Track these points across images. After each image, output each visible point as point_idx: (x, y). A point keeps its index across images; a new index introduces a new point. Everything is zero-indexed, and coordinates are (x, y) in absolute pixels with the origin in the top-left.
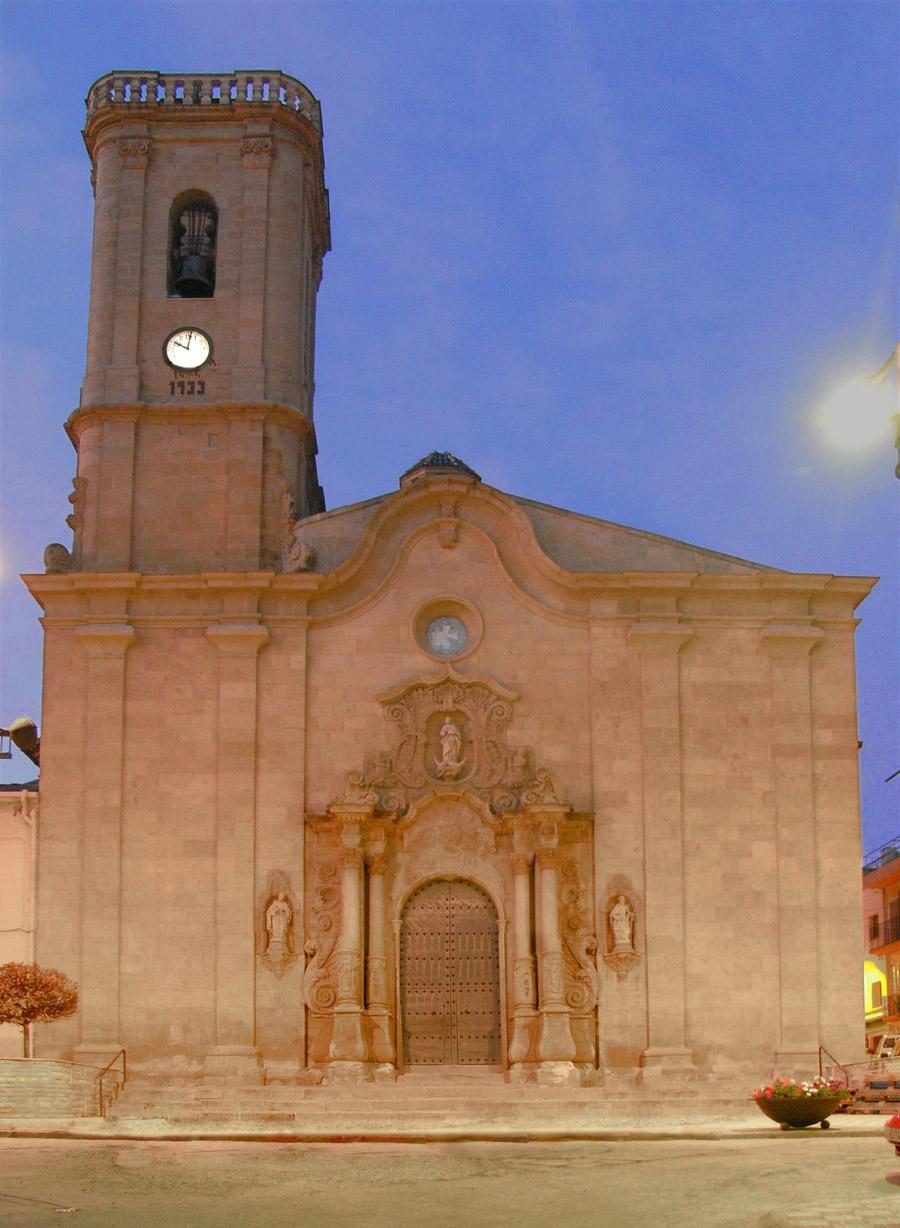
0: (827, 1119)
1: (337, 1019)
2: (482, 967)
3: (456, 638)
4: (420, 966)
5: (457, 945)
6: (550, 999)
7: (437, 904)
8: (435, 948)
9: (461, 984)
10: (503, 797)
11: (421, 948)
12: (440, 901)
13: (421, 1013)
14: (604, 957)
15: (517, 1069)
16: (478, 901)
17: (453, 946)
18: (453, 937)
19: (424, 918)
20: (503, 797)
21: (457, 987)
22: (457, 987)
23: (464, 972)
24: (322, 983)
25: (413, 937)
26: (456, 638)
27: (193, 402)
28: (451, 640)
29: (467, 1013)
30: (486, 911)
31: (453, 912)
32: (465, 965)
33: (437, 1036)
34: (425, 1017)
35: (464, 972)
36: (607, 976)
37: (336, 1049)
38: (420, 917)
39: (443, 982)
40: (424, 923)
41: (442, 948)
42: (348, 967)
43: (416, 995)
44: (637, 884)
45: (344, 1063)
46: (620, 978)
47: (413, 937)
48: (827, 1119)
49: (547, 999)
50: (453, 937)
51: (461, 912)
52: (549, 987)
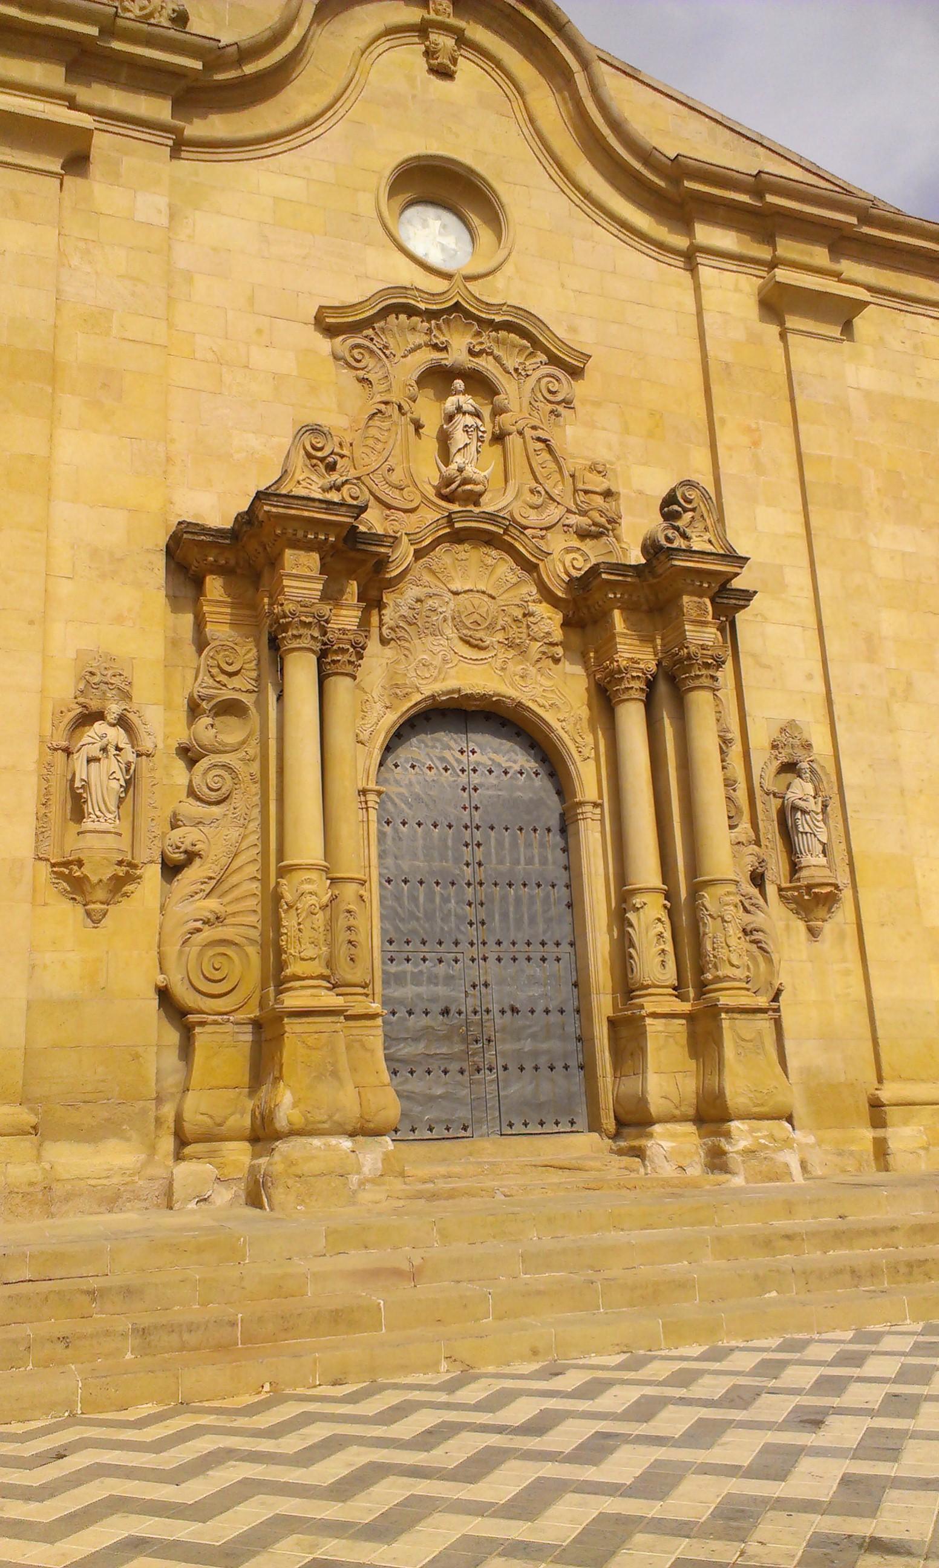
0: (644, 561)
1: (292, 1027)
2: (538, 907)
3: (453, 246)
4: (414, 899)
5: (487, 854)
6: (727, 978)
7: (442, 759)
8: (443, 858)
9: (499, 943)
10: (568, 550)
11: (415, 856)
12: (447, 754)
13: (418, 1010)
14: (780, 889)
15: (672, 1145)
16: (517, 759)
17: (479, 854)
18: (478, 835)
19: (417, 789)
20: (568, 550)
21: (492, 951)
22: (492, 951)
23: (505, 916)
24: (209, 934)
25: (396, 830)
26: (453, 246)
27: (459, 347)
28: (443, 248)
29: (514, 1010)
30: (538, 782)
31: (476, 779)
32: (504, 898)
33: (454, 1067)
34: (425, 1021)
35: (505, 916)
36: (788, 928)
37: (295, 1105)
38: (411, 784)
39: (460, 937)
40: (418, 798)
41: (457, 860)
42: (313, 900)
43: (409, 967)
44: (821, 745)
45: (310, 1140)
46: (813, 933)
47: (396, 830)
48: (644, 561)
49: (718, 979)
50: (478, 835)
51: (492, 780)
52: (723, 953)
